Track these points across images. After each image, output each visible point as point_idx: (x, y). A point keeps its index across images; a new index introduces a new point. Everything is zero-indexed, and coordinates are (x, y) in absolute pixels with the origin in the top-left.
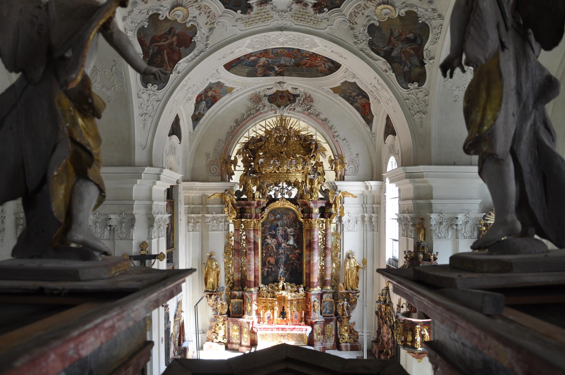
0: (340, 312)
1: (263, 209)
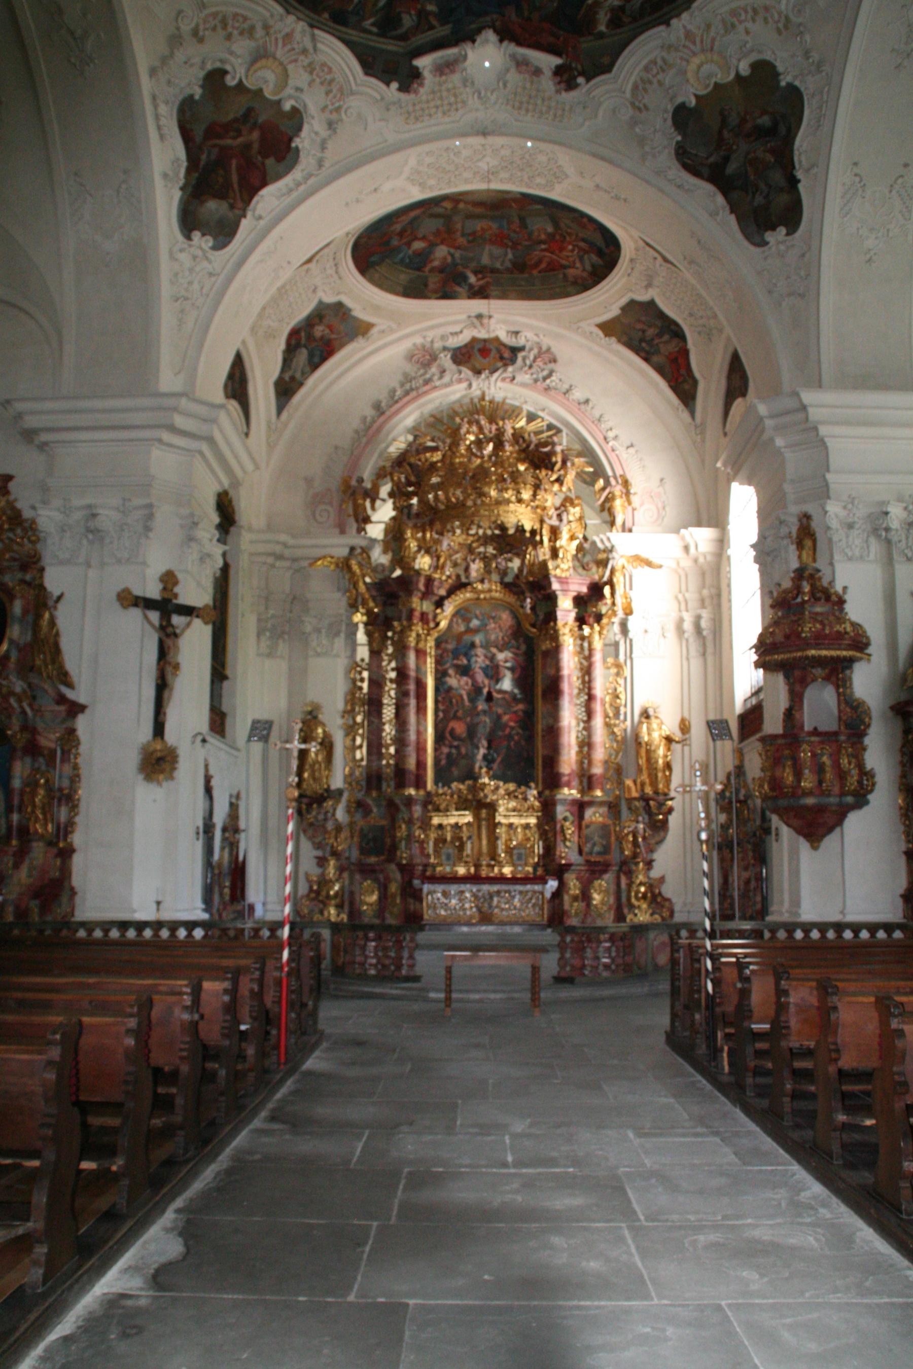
1: (439, 604)
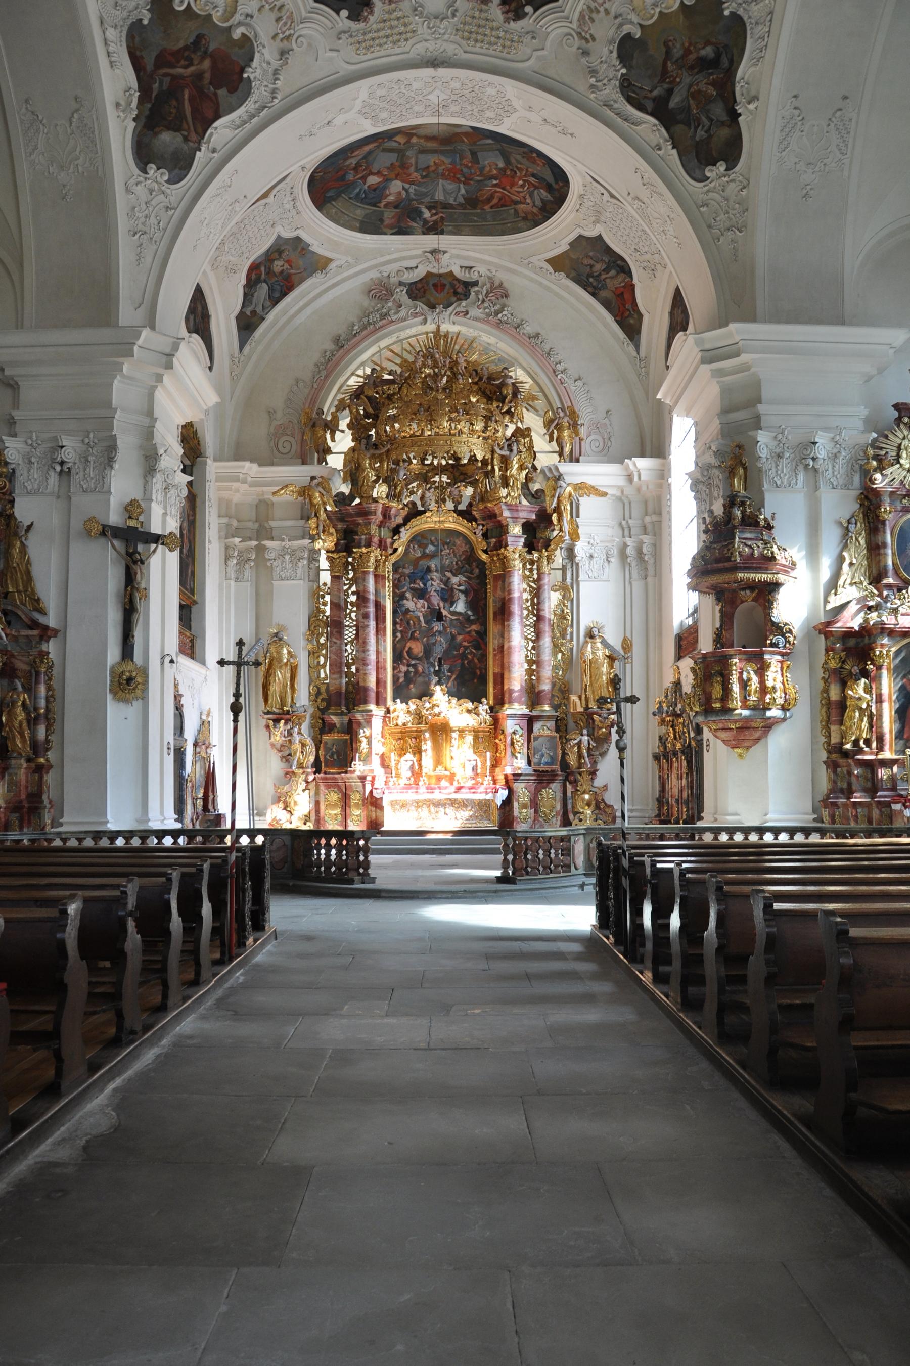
0: (572, 760)
1: (396, 531)
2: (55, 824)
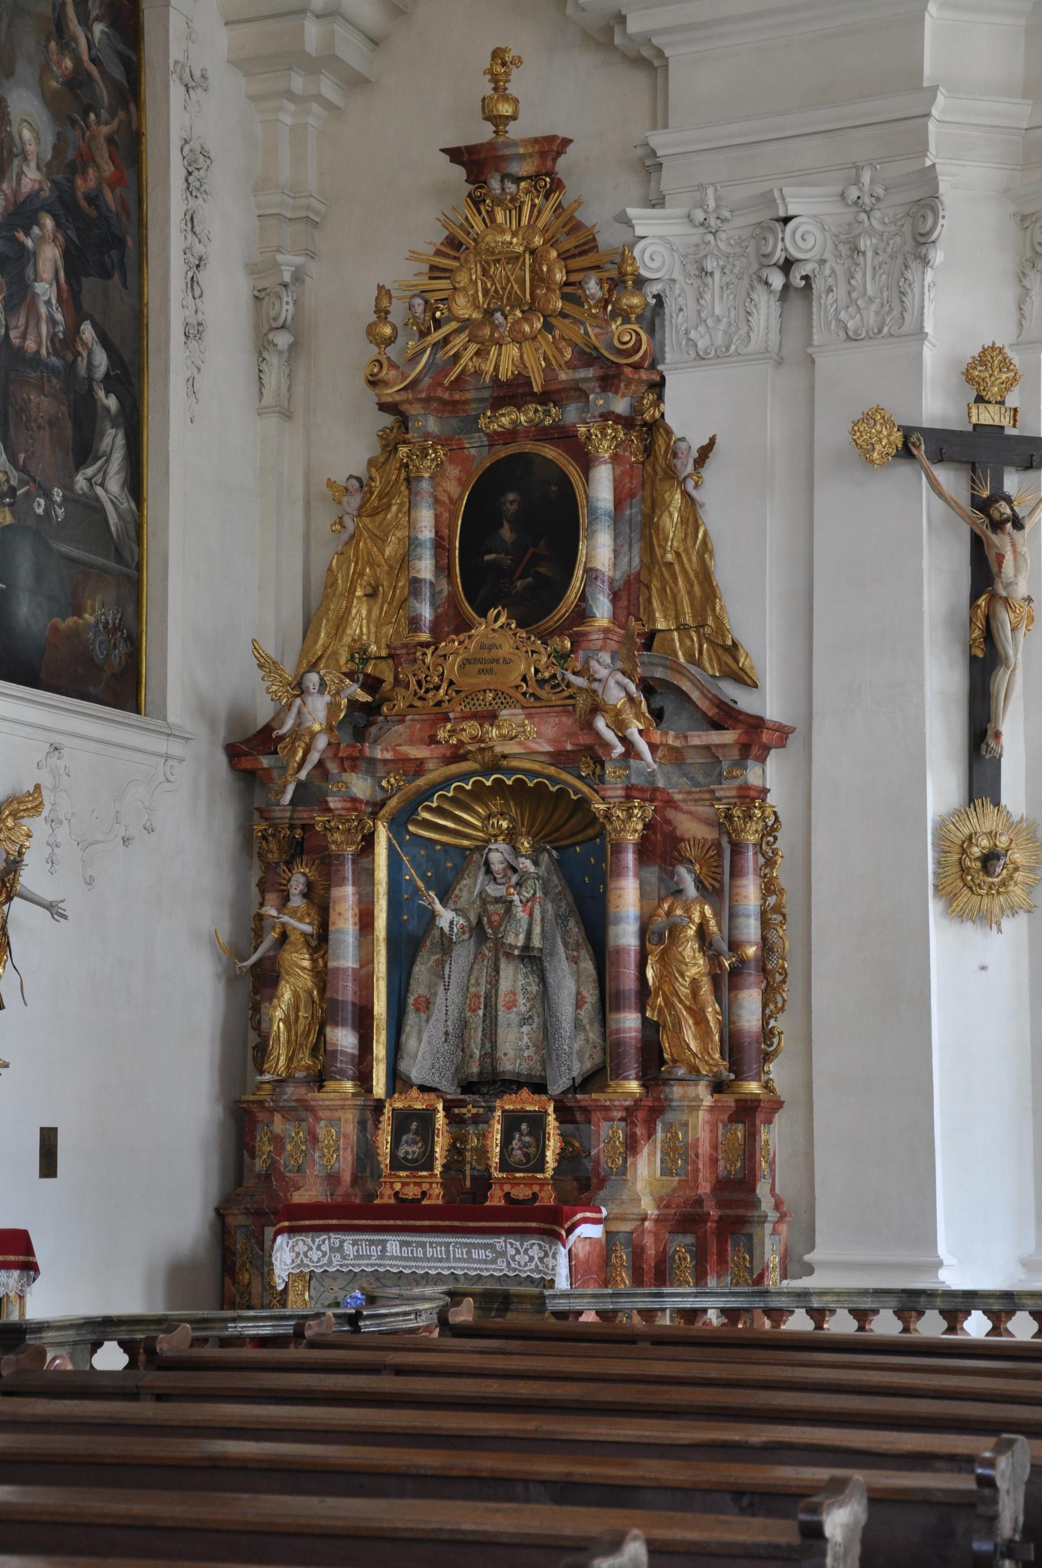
2: (792, 1268)
